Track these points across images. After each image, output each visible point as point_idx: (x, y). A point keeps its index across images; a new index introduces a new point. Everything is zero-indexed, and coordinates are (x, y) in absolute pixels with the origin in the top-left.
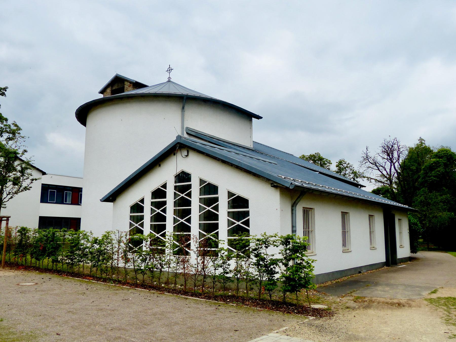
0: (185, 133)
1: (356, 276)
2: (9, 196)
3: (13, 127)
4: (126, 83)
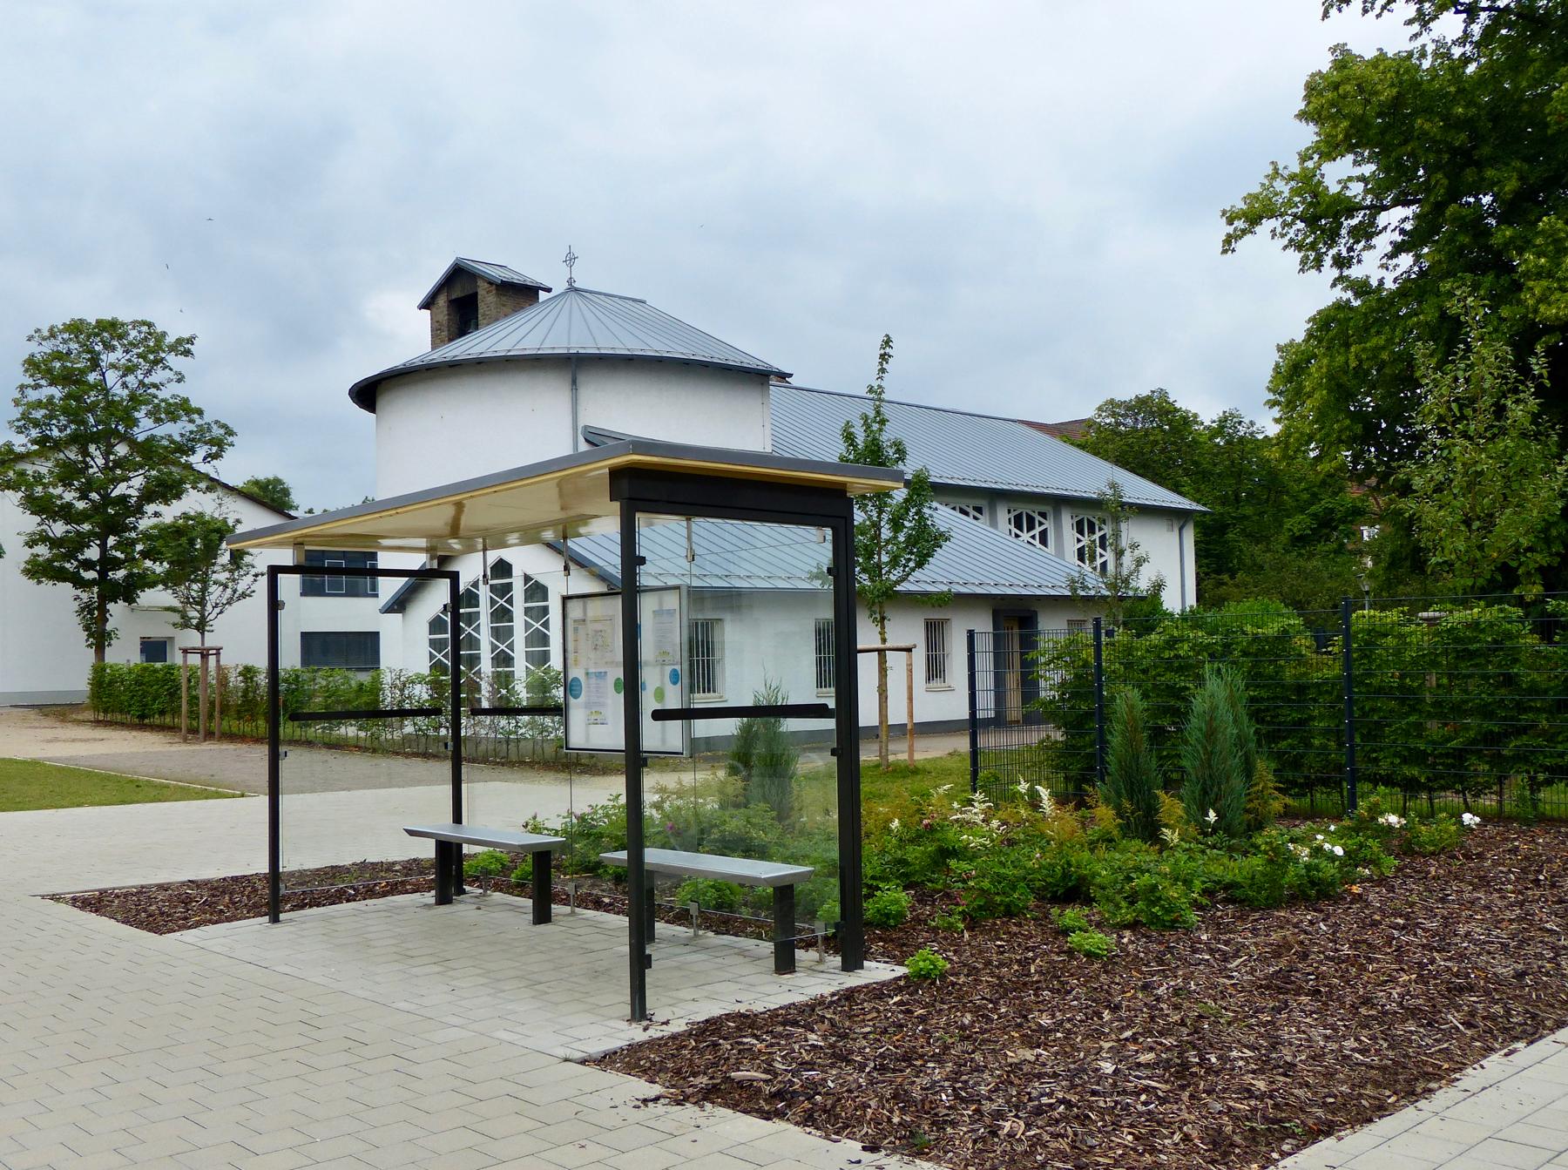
0: (581, 439)
1: (235, 725)
2: (217, 610)
3: (217, 432)
4: (480, 283)
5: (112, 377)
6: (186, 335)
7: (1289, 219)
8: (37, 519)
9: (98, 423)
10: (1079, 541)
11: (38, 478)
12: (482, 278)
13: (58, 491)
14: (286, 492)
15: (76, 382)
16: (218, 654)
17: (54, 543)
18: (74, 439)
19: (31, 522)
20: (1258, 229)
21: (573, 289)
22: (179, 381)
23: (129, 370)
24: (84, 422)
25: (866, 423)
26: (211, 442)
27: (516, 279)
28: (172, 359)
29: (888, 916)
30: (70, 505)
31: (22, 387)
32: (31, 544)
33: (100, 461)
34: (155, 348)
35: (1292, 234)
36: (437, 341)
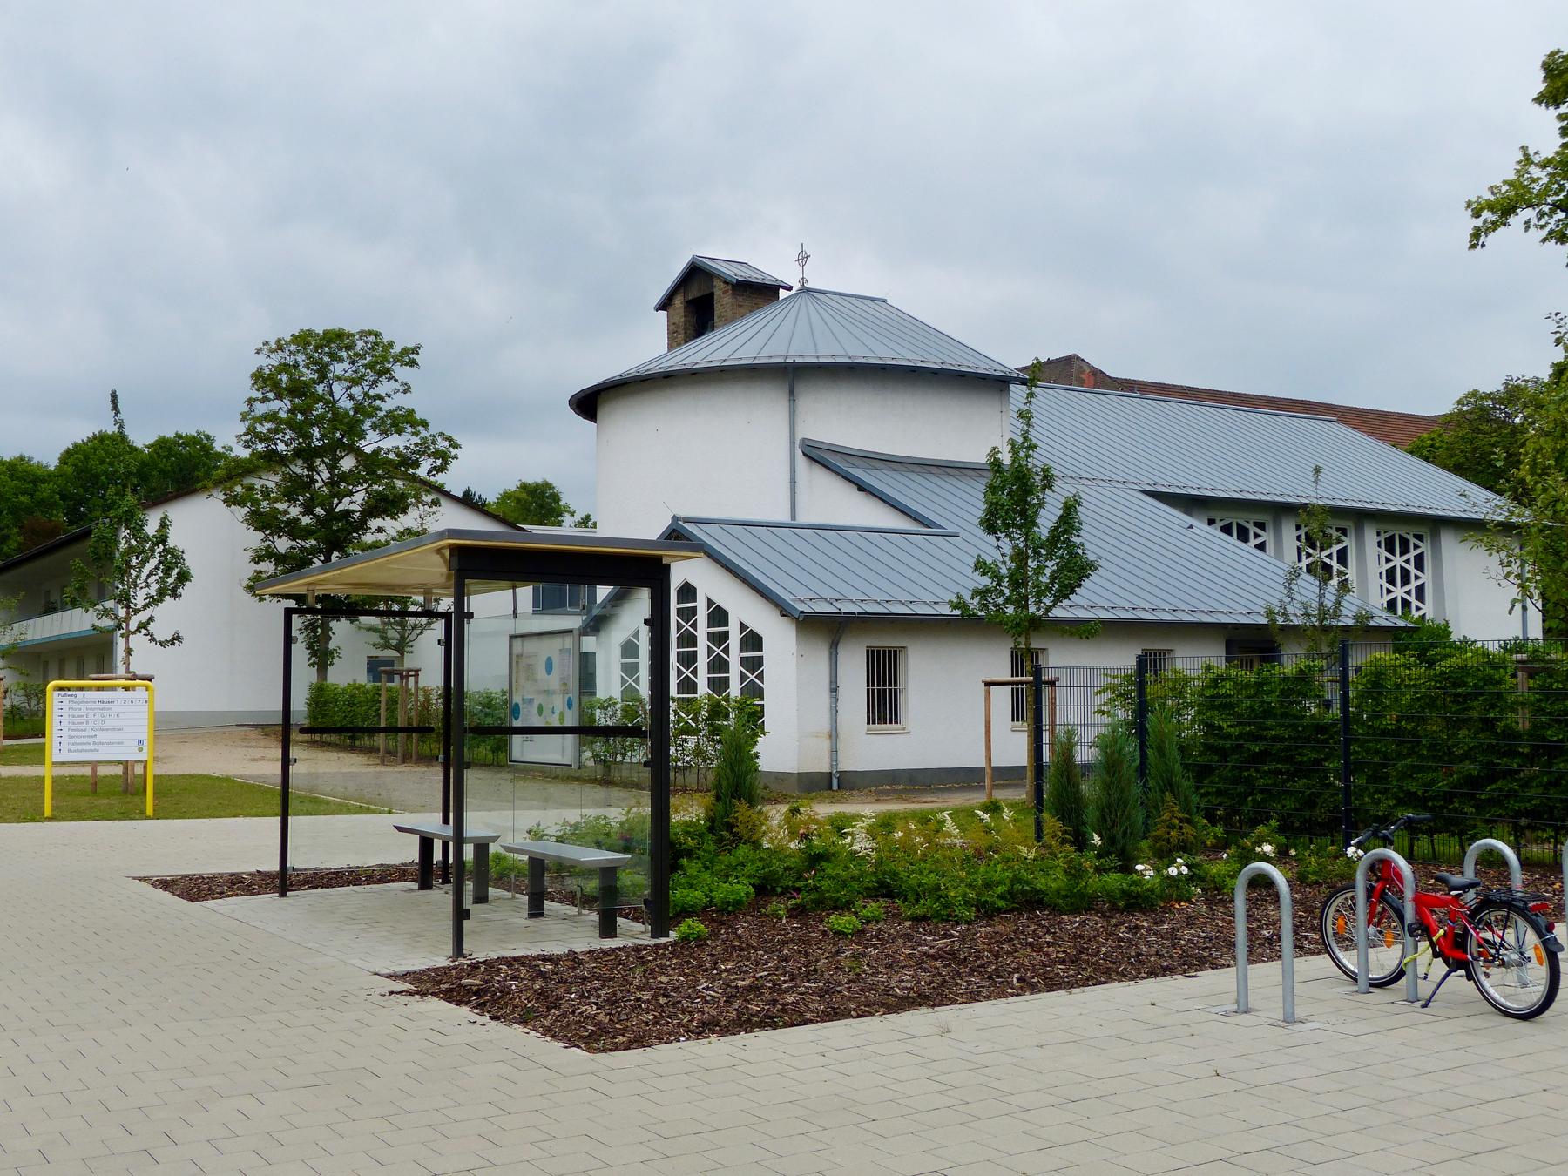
0: (799, 453)
3: (442, 444)
4: (717, 282)
5: (338, 389)
6: (411, 345)
7: (1546, 208)
8: (261, 535)
9: (323, 437)
10: (1388, 560)
11: (266, 492)
12: (718, 277)
13: (281, 506)
14: (556, 498)
15: (302, 395)
16: (416, 675)
17: (279, 559)
18: (297, 453)
19: (255, 539)
20: (1512, 219)
21: (805, 290)
22: (405, 392)
23: (355, 382)
24: (309, 437)
25: (1013, 446)
26: (436, 455)
27: (754, 277)
28: (400, 372)
29: (728, 903)
30: (296, 520)
31: (250, 401)
32: (257, 559)
33: (326, 475)
34: (382, 358)
35: (1552, 226)
36: (673, 343)
